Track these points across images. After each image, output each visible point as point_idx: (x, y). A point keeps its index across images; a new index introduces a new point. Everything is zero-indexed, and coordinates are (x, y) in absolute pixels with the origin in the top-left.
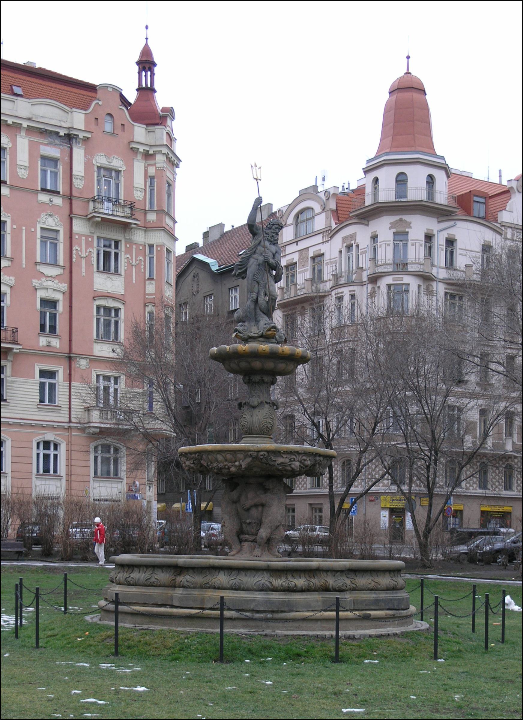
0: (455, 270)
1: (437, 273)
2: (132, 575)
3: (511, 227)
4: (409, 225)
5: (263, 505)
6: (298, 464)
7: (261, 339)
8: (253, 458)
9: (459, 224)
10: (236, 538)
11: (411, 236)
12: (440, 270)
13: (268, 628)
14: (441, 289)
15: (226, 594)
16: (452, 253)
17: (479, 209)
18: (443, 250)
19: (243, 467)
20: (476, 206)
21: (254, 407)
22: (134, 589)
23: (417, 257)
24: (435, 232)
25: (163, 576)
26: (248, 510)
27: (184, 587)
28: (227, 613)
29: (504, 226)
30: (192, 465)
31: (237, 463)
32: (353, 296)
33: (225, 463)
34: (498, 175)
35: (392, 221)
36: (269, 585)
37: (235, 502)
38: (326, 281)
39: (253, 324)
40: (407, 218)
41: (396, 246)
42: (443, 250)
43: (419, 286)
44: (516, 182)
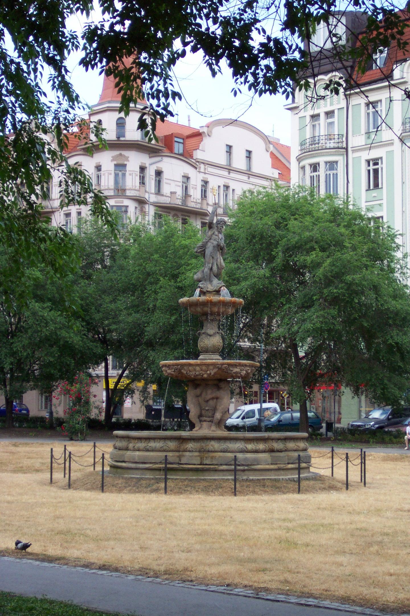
0: (163, 195)
1: (149, 198)
2: (149, 445)
3: (204, 163)
4: (127, 159)
5: (217, 398)
6: (245, 372)
7: (214, 293)
8: (219, 369)
9: (165, 159)
10: (198, 420)
11: (128, 168)
12: (151, 196)
13: (245, 475)
14: (151, 211)
15: (240, 456)
16: (159, 182)
17: (178, 148)
18: (153, 179)
19: (212, 374)
20: (176, 145)
21: (210, 336)
22: (152, 454)
23: (134, 185)
24: (147, 165)
25: (172, 445)
26: (207, 401)
27: (189, 451)
28: (238, 468)
29: (198, 162)
30: (173, 373)
31: (208, 372)
32: (79, 213)
33: (201, 372)
34: (188, 119)
35: (114, 155)
36: (245, 448)
37: (197, 396)
38: (54, 200)
39: (208, 283)
40: (126, 153)
41: (116, 175)
42: (153, 179)
43: (136, 208)
44: (207, 128)
